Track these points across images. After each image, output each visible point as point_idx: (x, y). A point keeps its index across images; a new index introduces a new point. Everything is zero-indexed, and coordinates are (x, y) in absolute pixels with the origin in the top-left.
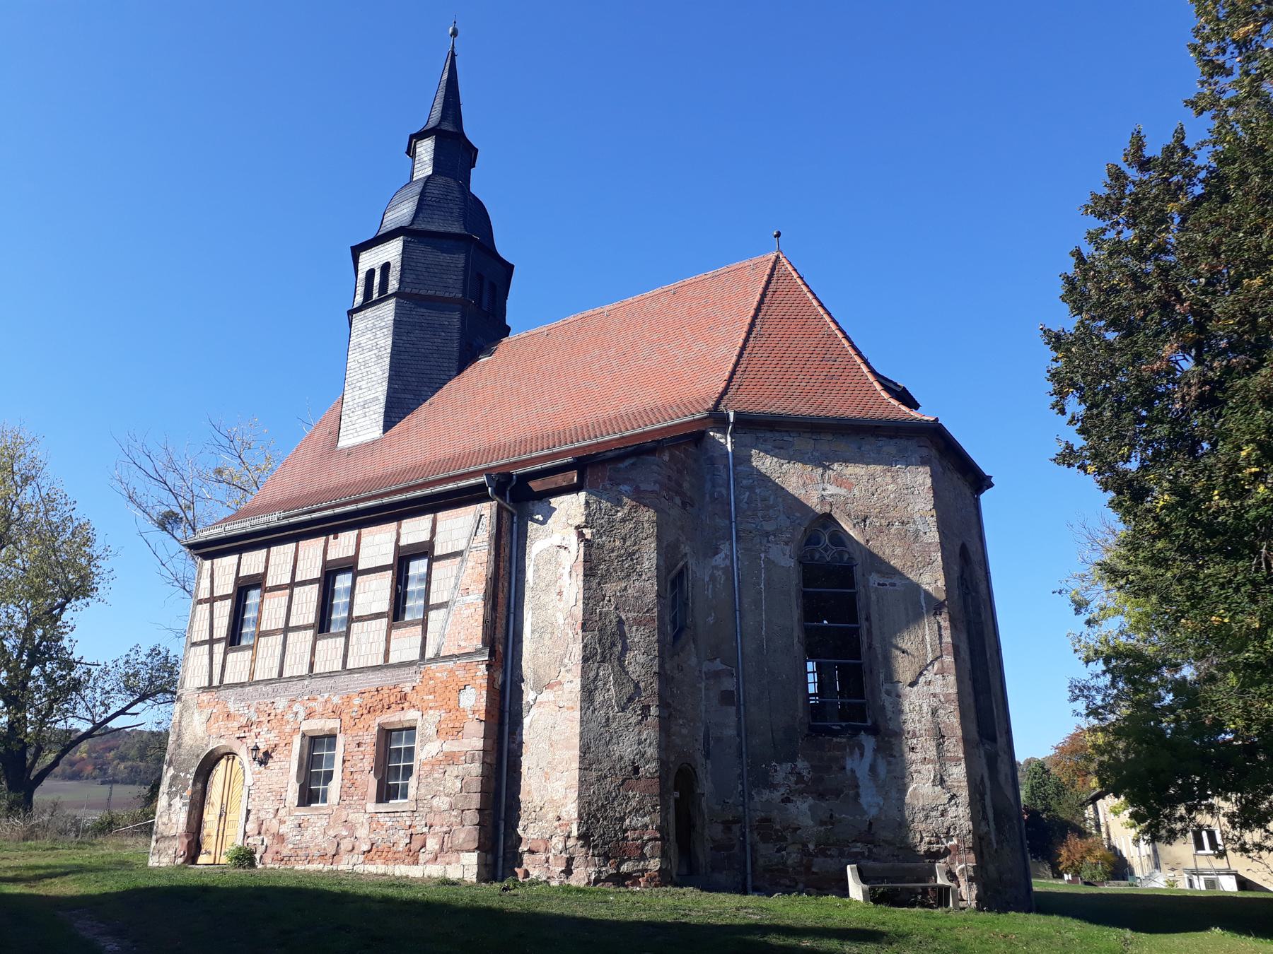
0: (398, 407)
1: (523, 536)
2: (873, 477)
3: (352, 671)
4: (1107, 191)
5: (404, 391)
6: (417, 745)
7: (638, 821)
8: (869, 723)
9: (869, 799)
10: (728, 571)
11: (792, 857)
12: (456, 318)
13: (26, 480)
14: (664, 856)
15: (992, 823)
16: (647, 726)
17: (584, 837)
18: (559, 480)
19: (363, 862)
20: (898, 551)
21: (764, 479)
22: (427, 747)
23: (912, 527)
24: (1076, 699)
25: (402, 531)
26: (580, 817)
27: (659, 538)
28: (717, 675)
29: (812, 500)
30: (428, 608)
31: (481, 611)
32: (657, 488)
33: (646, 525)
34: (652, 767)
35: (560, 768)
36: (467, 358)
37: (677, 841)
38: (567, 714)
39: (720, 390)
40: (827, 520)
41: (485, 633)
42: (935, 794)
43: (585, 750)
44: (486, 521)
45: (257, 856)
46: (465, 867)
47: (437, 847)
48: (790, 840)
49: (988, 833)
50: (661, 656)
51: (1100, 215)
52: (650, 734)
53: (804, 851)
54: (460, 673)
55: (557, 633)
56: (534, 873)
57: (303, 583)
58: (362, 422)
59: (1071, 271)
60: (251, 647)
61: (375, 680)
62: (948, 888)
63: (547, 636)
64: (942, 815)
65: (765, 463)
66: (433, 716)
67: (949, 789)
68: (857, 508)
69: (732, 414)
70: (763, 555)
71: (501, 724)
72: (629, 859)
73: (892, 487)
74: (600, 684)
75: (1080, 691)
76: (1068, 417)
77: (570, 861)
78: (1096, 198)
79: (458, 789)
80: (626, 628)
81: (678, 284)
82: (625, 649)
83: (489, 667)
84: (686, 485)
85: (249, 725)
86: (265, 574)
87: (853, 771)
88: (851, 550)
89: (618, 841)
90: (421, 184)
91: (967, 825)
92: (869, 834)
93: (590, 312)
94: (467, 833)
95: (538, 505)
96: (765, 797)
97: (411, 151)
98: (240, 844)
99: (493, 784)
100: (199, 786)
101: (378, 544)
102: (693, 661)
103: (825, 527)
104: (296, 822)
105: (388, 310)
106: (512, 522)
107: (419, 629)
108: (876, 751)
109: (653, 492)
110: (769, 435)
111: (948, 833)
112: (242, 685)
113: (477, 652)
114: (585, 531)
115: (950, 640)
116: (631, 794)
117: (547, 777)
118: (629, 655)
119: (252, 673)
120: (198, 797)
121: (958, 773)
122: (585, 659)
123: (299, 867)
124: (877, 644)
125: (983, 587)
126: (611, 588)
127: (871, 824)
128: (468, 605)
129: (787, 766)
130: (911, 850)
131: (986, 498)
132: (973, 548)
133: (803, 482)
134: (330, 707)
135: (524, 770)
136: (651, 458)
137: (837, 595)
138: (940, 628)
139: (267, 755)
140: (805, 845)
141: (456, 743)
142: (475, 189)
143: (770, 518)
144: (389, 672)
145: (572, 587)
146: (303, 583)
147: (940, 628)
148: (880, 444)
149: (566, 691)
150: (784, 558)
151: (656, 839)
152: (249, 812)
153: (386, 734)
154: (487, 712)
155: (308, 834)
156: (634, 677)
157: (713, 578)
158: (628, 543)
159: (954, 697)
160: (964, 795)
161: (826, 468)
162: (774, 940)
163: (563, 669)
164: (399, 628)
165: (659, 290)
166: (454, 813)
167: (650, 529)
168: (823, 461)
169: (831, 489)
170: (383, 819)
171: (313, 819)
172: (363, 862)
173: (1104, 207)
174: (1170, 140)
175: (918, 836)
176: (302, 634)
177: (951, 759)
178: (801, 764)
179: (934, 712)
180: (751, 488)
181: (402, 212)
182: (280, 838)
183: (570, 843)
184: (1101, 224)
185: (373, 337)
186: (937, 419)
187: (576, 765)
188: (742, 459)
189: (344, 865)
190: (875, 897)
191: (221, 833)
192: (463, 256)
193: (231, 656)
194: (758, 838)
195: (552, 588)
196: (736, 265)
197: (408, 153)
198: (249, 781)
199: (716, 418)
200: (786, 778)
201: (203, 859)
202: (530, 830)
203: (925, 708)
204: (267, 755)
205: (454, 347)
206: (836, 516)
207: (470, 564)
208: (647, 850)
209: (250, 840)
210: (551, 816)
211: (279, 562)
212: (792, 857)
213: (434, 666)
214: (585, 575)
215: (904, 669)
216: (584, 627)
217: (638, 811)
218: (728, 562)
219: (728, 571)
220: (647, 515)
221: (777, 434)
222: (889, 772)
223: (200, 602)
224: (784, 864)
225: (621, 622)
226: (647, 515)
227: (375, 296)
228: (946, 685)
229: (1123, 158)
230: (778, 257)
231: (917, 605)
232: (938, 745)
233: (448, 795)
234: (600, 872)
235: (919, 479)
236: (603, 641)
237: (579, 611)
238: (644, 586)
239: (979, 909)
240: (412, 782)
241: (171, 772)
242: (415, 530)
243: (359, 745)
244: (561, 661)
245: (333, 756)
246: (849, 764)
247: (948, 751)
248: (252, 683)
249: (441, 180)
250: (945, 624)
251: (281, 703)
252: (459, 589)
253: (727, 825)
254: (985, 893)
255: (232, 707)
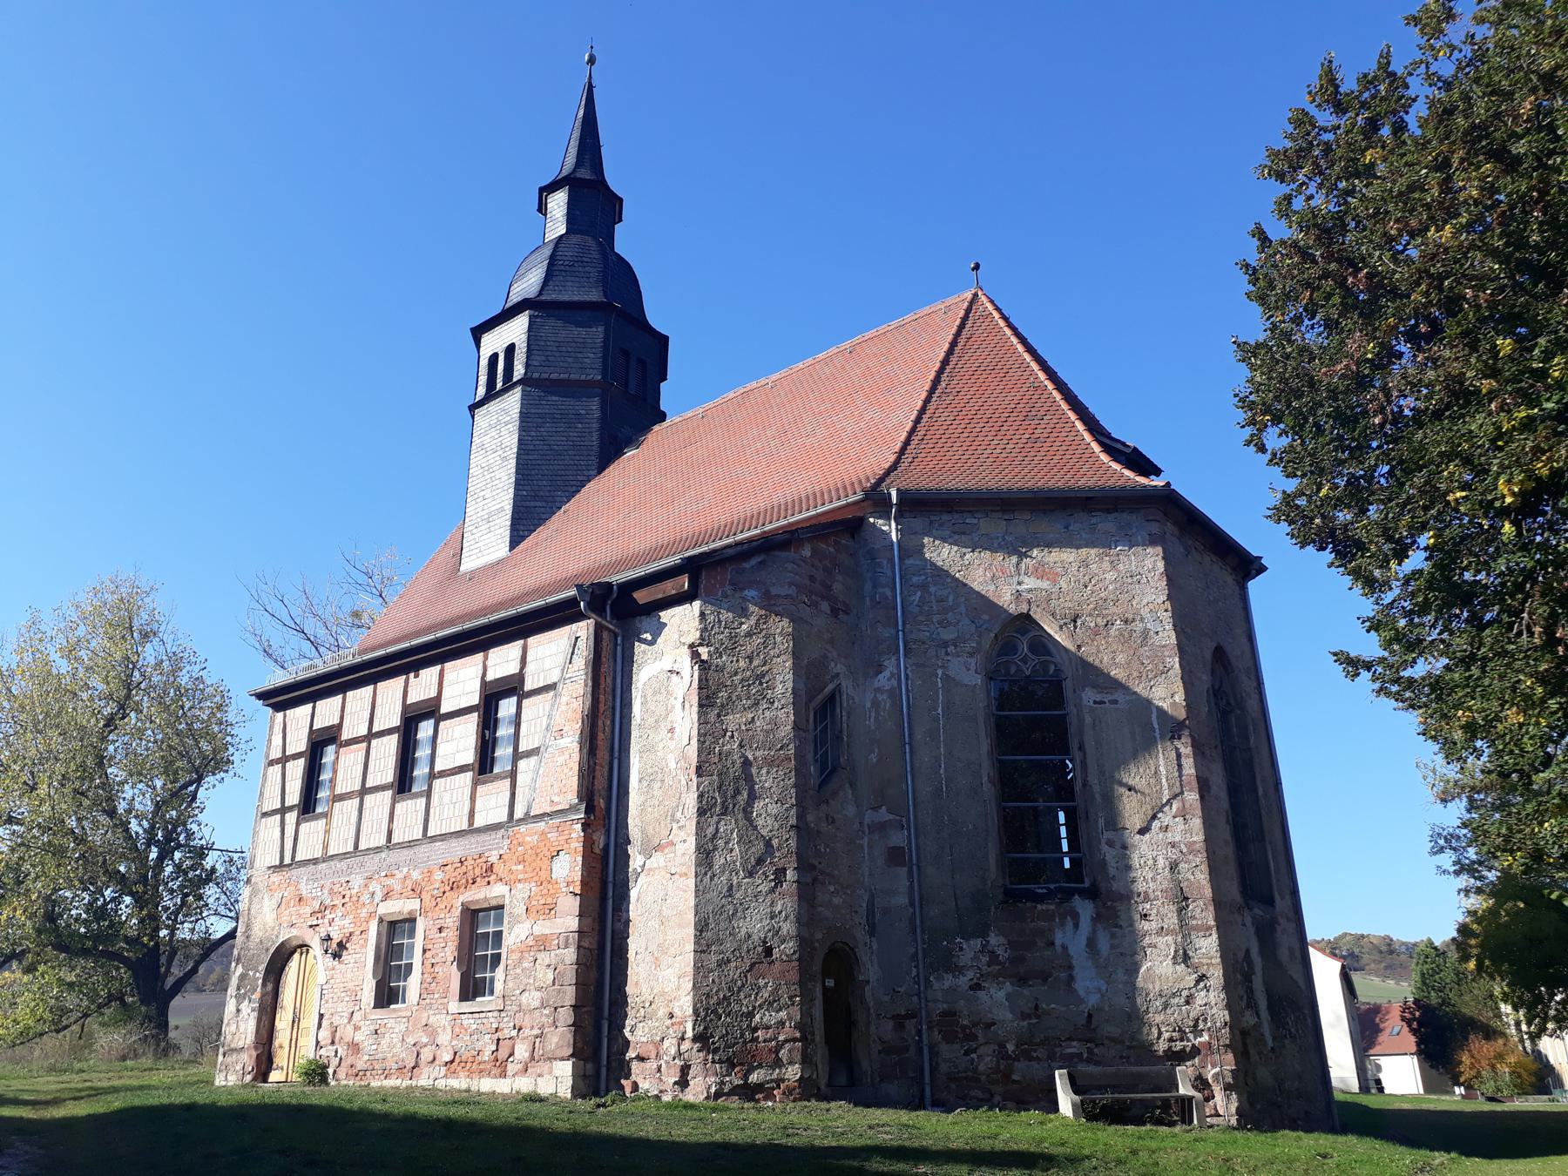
0: (525, 521)
1: (628, 661)
2: (1085, 563)
3: (434, 839)
4: (1289, 144)
5: (535, 497)
6: (505, 928)
7: (771, 1017)
8: (1087, 884)
9: (1087, 983)
10: (894, 694)
11: (986, 1060)
12: (594, 405)
13: (146, 636)
14: (806, 1060)
15: (1265, 1014)
16: (782, 895)
17: (701, 1038)
18: (669, 588)
19: (445, 1076)
20: (1121, 658)
21: (940, 574)
22: (516, 930)
23: (1138, 626)
24: (1442, 850)
25: (489, 663)
26: (696, 1012)
27: (796, 655)
28: (882, 827)
29: (1004, 597)
30: (517, 756)
31: (576, 757)
32: (792, 591)
33: (778, 639)
34: (790, 946)
35: (672, 951)
36: (610, 451)
37: (828, 1040)
38: (681, 882)
39: (887, 466)
40: (1025, 622)
41: (580, 785)
42: (1178, 973)
43: (701, 927)
44: (582, 644)
45: (330, 1071)
46: (558, 1079)
47: (527, 1055)
48: (981, 1039)
49: (1258, 1026)
50: (800, 804)
51: (1280, 177)
52: (786, 904)
53: (1002, 1054)
54: (552, 836)
55: (669, 781)
56: (644, 1085)
57: (382, 734)
58: (486, 541)
59: (1254, 258)
60: (325, 815)
61: (458, 848)
62: (1191, 1099)
63: (657, 785)
64: (1187, 1003)
65: (942, 554)
66: (522, 890)
67: (1196, 968)
68: (1065, 605)
69: (894, 494)
70: (940, 672)
71: (603, 899)
72: (760, 1066)
73: (1110, 576)
74: (721, 843)
75: (1444, 842)
76: (1268, 456)
77: (685, 1069)
78: (1274, 154)
79: (550, 982)
80: (754, 770)
81: (855, 340)
82: (753, 797)
83: (585, 826)
84: (837, 587)
85: (322, 910)
86: (340, 726)
87: (1064, 947)
88: (1058, 660)
89: (745, 1043)
90: (551, 246)
91: (1221, 1015)
92: (1088, 1029)
93: (754, 384)
94: (560, 1037)
95: (645, 622)
96: (947, 984)
97: (542, 208)
98: (312, 1056)
99: (593, 974)
100: (270, 987)
101: (461, 681)
102: (851, 811)
103: (1024, 632)
104: (372, 1028)
105: (512, 402)
106: (616, 644)
107: (507, 782)
108: (1097, 919)
109: (787, 596)
110: (946, 517)
111: (1196, 1026)
112: (315, 861)
113: (572, 809)
114: (700, 650)
115: (1193, 771)
116: (761, 982)
117: (657, 963)
118: (758, 805)
119: (326, 847)
120: (269, 999)
121: (1208, 946)
122: (701, 812)
123: (375, 1084)
124: (1093, 780)
125: (1252, 703)
126: (733, 721)
127: (1090, 1016)
128: (562, 751)
129: (977, 943)
130: (1146, 1050)
131: (1254, 586)
132: (1235, 652)
133: (992, 576)
134: (409, 883)
135: (631, 955)
136: (784, 554)
137: (1040, 714)
138: (1179, 756)
139: (342, 946)
140: (1002, 1046)
141: (547, 923)
142: (620, 247)
143: (949, 624)
144: (474, 839)
145: (686, 722)
146: (382, 734)
147: (1179, 756)
148: (1094, 520)
149: (679, 853)
150: (968, 673)
151: (795, 1040)
152: (321, 1016)
153: (472, 916)
154: (584, 883)
155: (385, 1042)
156: (764, 832)
157: (875, 703)
158: (756, 663)
159: (1200, 846)
160: (1216, 975)
161: (1021, 556)
162: (876, 1165)
163: (675, 826)
164: (485, 783)
165: (834, 350)
166: (546, 1012)
167: (783, 644)
168: (1017, 547)
169: (1030, 583)
170: (467, 1021)
171: (391, 1022)
172: (445, 1076)
173: (1283, 166)
174: (1371, 67)
175: (1155, 1031)
176: (380, 795)
177: (1197, 928)
178: (994, 939)
179: (1174, 867)
180: (924, 587)
181: (529, 283)
182: (355, 1047)
183: (684, 1047)
184: (1285, 189)
185: (498, 432)
186: (1168, 484)
187: (690, 947)
188: (911, 550)
189: (423, 1081)
190: (1091, 1112)
191: (294, 1043)
192: (601, 329)
193: (304, 827)
194: (937, 1037)
195: (662, 724)
196: (927, 310)
197: (540, 210)
198: (321, 979)
199: (875, 498)
200: (975, 958)
201: (275, 1076)
202: (639, 1032)
203: (1161, 862)
204: (342, 946)
205: (594, 440)
206: (1037, 617)
207: (564, 699)
208: (783, 1053)
209: (322, 1052)
210: (662, 1012)
211: (352, 710)
212: (986, 1060)
213: (523, 829)
214: (701, 706)
215: (1132, 812)
216: (699, 771)
217: (771, 1004)
218: (894, 682)
219: (894, 694)
220: (781, 627)
221: (956, 516)
222: (1112, 947)
223: (272, 763)
224: (975, 1070)
225: (747, 763)
226: (781, 627)
227: (499, 385)
228: (1189, 831)
229: (1308, 98)
230: (976, 295)
231: (1150, 728)
232: (1180, 911)
233: (539, 989)
234: (722, 1083)
235: (1149, 563)
236: (723, 788)
237: (693, 752)
238: (775, 715)
239: (1241, 1126)
240: (499, 973)
241: (240, 970)
242: (502, 661)
243: (440, 930)
244: (673, 819)
245: (412, 945)
246: (1059, 938)
247: (1193, 917)
248: (326, 859)
249: (576, 239)
250: (1187, 750)
251: (357, 881)
252: (551, 729)
253: (899, 1021)
254: (1251, 1104)
255: (304, 889)
